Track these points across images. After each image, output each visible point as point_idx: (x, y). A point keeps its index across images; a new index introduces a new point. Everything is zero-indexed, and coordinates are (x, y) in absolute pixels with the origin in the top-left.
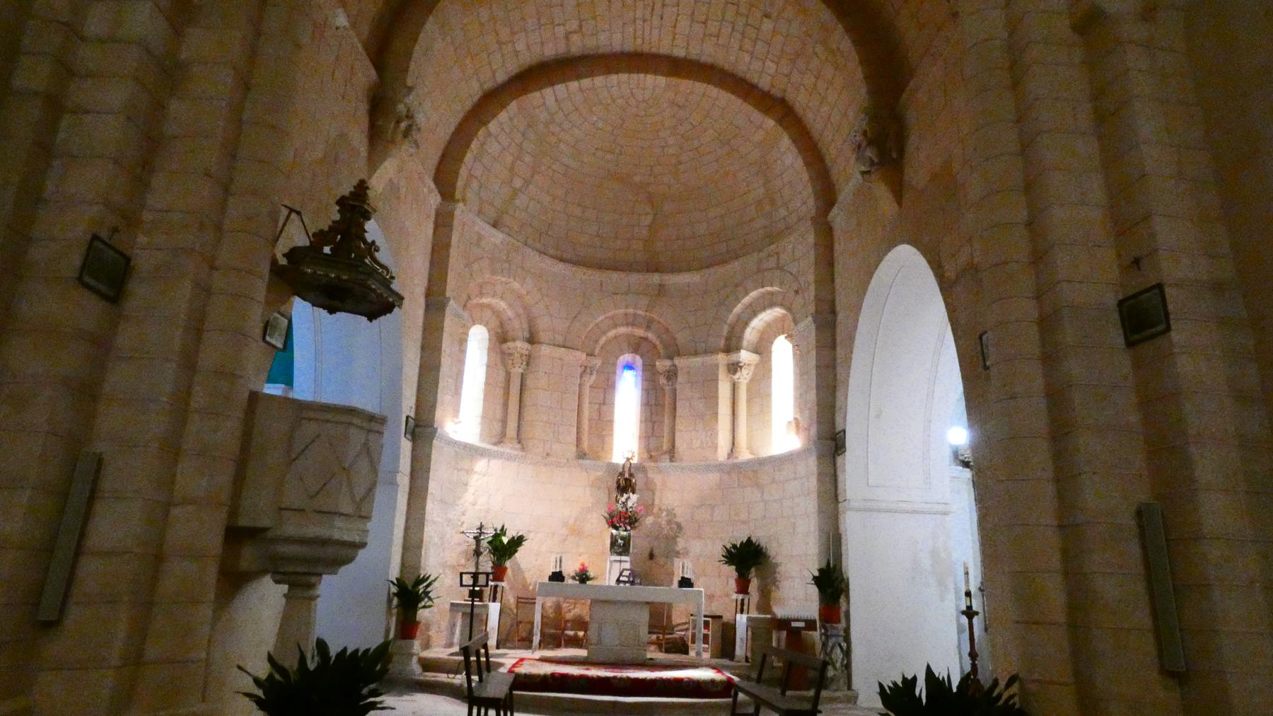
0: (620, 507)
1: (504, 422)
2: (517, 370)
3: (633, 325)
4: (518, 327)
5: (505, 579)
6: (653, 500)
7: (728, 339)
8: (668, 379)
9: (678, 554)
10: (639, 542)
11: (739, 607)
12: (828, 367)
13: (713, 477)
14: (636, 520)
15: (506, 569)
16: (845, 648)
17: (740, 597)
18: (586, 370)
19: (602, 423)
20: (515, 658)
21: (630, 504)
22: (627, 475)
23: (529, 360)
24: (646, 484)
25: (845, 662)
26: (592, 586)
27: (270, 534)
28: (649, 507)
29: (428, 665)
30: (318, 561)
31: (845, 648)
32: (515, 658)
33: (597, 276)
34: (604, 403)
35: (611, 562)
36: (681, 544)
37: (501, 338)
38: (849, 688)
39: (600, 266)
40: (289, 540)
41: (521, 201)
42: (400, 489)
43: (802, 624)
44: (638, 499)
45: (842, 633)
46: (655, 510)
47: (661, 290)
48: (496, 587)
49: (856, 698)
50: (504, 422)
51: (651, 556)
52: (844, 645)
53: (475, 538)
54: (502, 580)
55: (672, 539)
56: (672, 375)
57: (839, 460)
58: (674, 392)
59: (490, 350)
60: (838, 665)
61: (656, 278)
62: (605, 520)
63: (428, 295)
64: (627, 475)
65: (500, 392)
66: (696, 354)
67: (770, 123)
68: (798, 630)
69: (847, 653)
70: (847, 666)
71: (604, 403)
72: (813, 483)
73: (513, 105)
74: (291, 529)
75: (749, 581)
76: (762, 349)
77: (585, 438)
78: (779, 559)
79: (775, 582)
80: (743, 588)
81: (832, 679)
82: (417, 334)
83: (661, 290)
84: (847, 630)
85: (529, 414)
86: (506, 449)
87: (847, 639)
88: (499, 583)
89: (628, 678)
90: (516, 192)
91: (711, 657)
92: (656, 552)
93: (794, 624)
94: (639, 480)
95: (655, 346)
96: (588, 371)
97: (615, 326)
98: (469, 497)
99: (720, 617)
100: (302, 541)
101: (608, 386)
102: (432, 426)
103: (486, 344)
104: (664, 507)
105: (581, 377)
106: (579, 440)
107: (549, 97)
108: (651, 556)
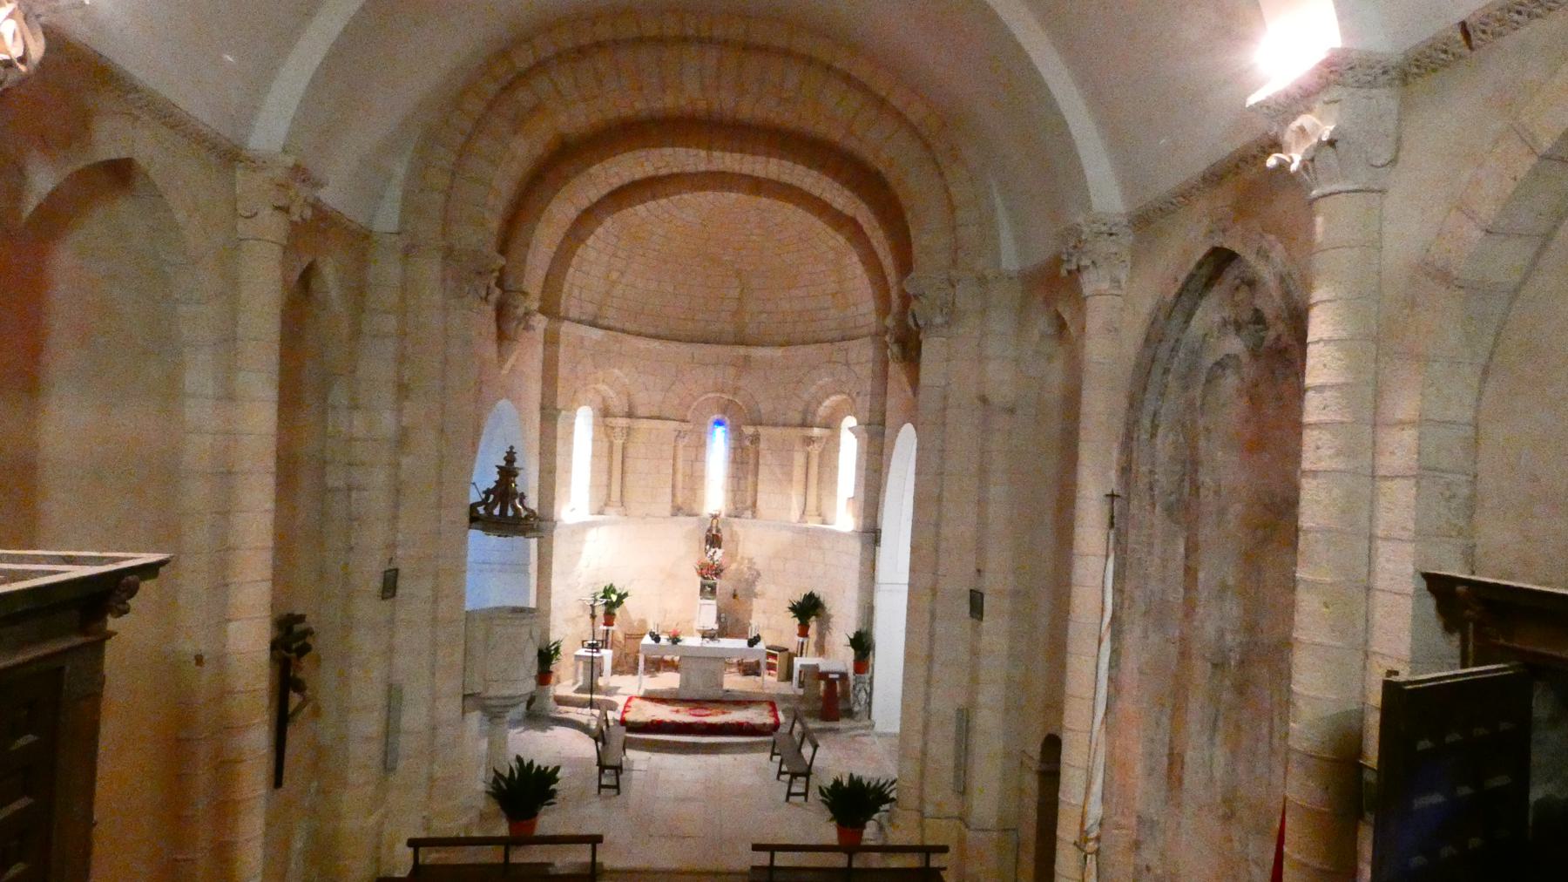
0: (707, 560)
1: (609, 486)
2: (618, 442)
3: (723, 391)
4: (617, 404)
5: (615, 623)
6: (737, 550)
7: (805, 412)
8: (752, 442)
9: (756, 595)
10: (722, 584)
11: (805, 647)
12: (875, 471)
13: (786, 536)
14: (722, 571)
15: (614, 614)
16: (868, 691)
17: (801, 639)
18: (679, 435)
19: (695, 479)
20: (625, 695)
21: (716, 558)
22: (714, 532)
23: (629, 431)
24: (731, 536)
25: (868, 700)
26: (680, 646)
27: (482, 696)
28: (732, 556)
29: (560, 701)
30: (506, 706)
31: (868, 691)
32: (625, 695)
33: (685, 349)
34: (696, 459)
35: (701, 605)
36: (758, 588)
37: (605, 413)
38: (869, 718)
39: (691, 340)
40: (490, 698)
41: (618, 290)
42: (531, 576)
43: (837, 676)
44: (724, 553)
45: (868, 681)
46: (739, 557)
47: (747, 358)
48: (607, 631)
49: (873, 726)
50: (609, 486)
51: (735, 596)
52: (868, 689)
53: (591, 605)
54: (612, 625)
55: (751, 584)
56: (755, 439)
57: (877, 548)
58: (757, 453)
59: (596, 425)
60: (863, 703)
61: (742, 350)
62: (695, 570)
63: (543, 408)
64: (714, 532)
65: (605, 461)
66: (775, 425)
67: (841, 239)
68: (834, 681)
69: (870, 695)
70: (869, 704)
71: (696, 459)
72: (856, 563)
73: (608, 222)
74: (491, 693)
75: (808, 627)
76: (832, 424)
77: (679, 494)
78: (832, 612)
79: (828, 628)
80: (804, 632)
81: (857, 713)
82: (536, 449)
83: (746, 363)
84: (871, 679)
85: (630, 478)
86: (612, 514)
87: (871, 683)
88: (611, 628)
89: (705, 724)
90: (614, 284)
91: (778, 681)
92: (738, 592)
93: (831, 676)
94: (725, 535)
95: (741, 408)
96: (682, 434)
97: (706, 393)
98: (582, 563)
99: (787, 650)
100: (497, 698)
101: (700, 446)
102: (552, 520)
103: (590, 421)
104: (745, 556)
105: (676, 441)
106: (674, 495)
107: (641, 211)
108: (735, 596)
